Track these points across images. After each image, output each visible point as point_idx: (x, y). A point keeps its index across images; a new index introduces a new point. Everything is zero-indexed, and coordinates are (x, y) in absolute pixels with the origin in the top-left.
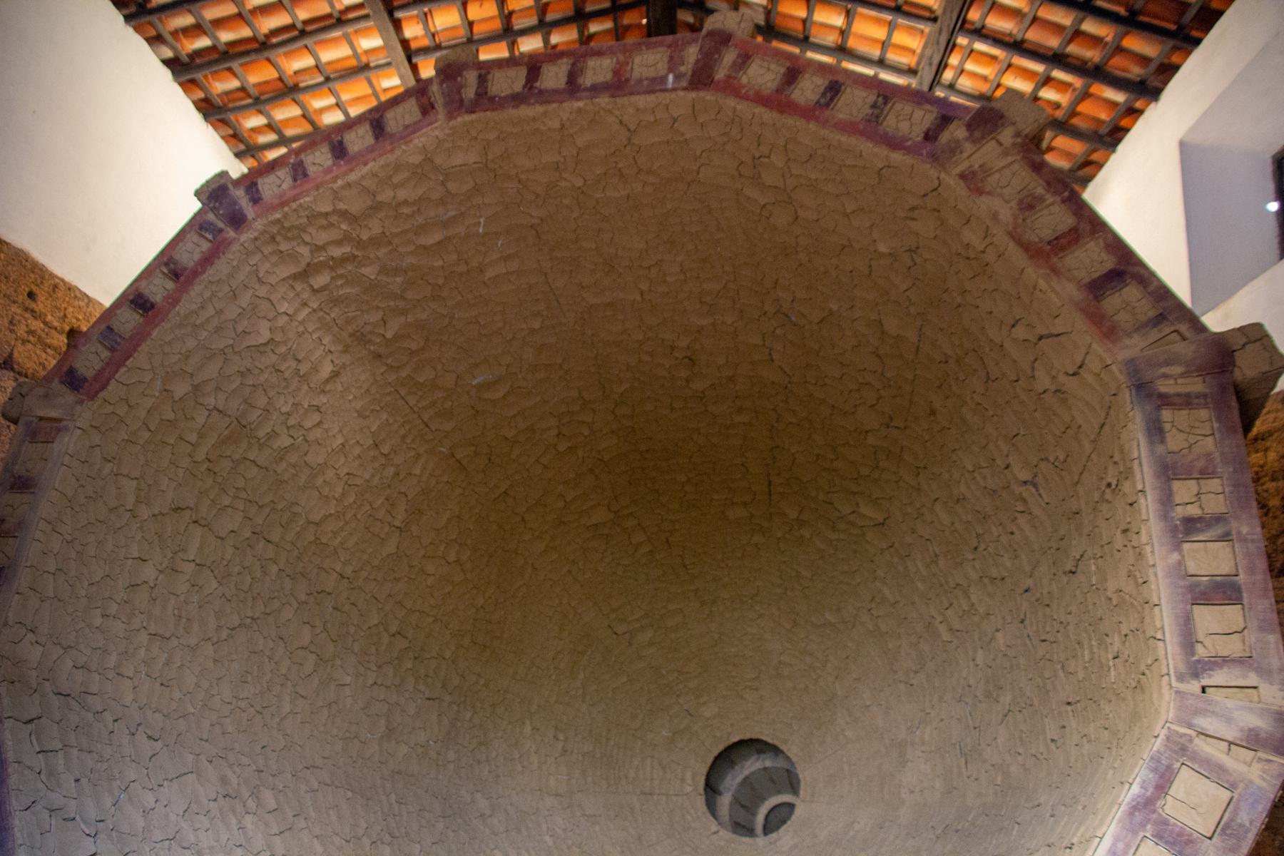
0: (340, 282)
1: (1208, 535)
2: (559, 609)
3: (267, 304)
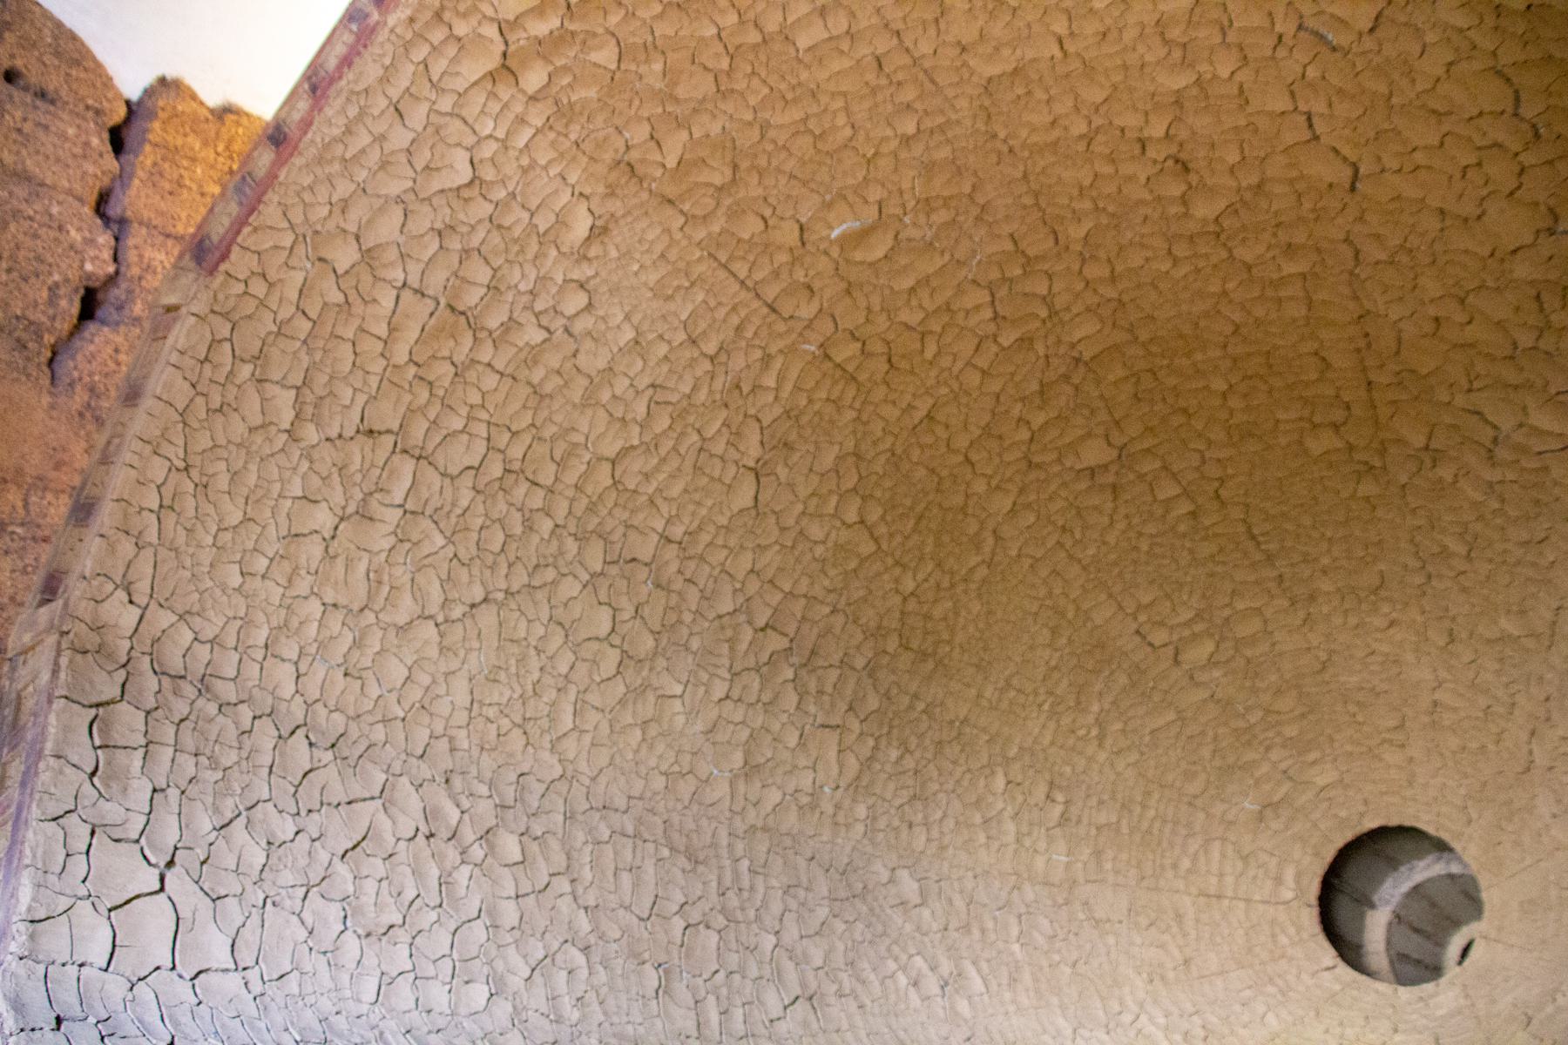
0: (566, 80)
2: (1048, 602)
3: (458, 123)
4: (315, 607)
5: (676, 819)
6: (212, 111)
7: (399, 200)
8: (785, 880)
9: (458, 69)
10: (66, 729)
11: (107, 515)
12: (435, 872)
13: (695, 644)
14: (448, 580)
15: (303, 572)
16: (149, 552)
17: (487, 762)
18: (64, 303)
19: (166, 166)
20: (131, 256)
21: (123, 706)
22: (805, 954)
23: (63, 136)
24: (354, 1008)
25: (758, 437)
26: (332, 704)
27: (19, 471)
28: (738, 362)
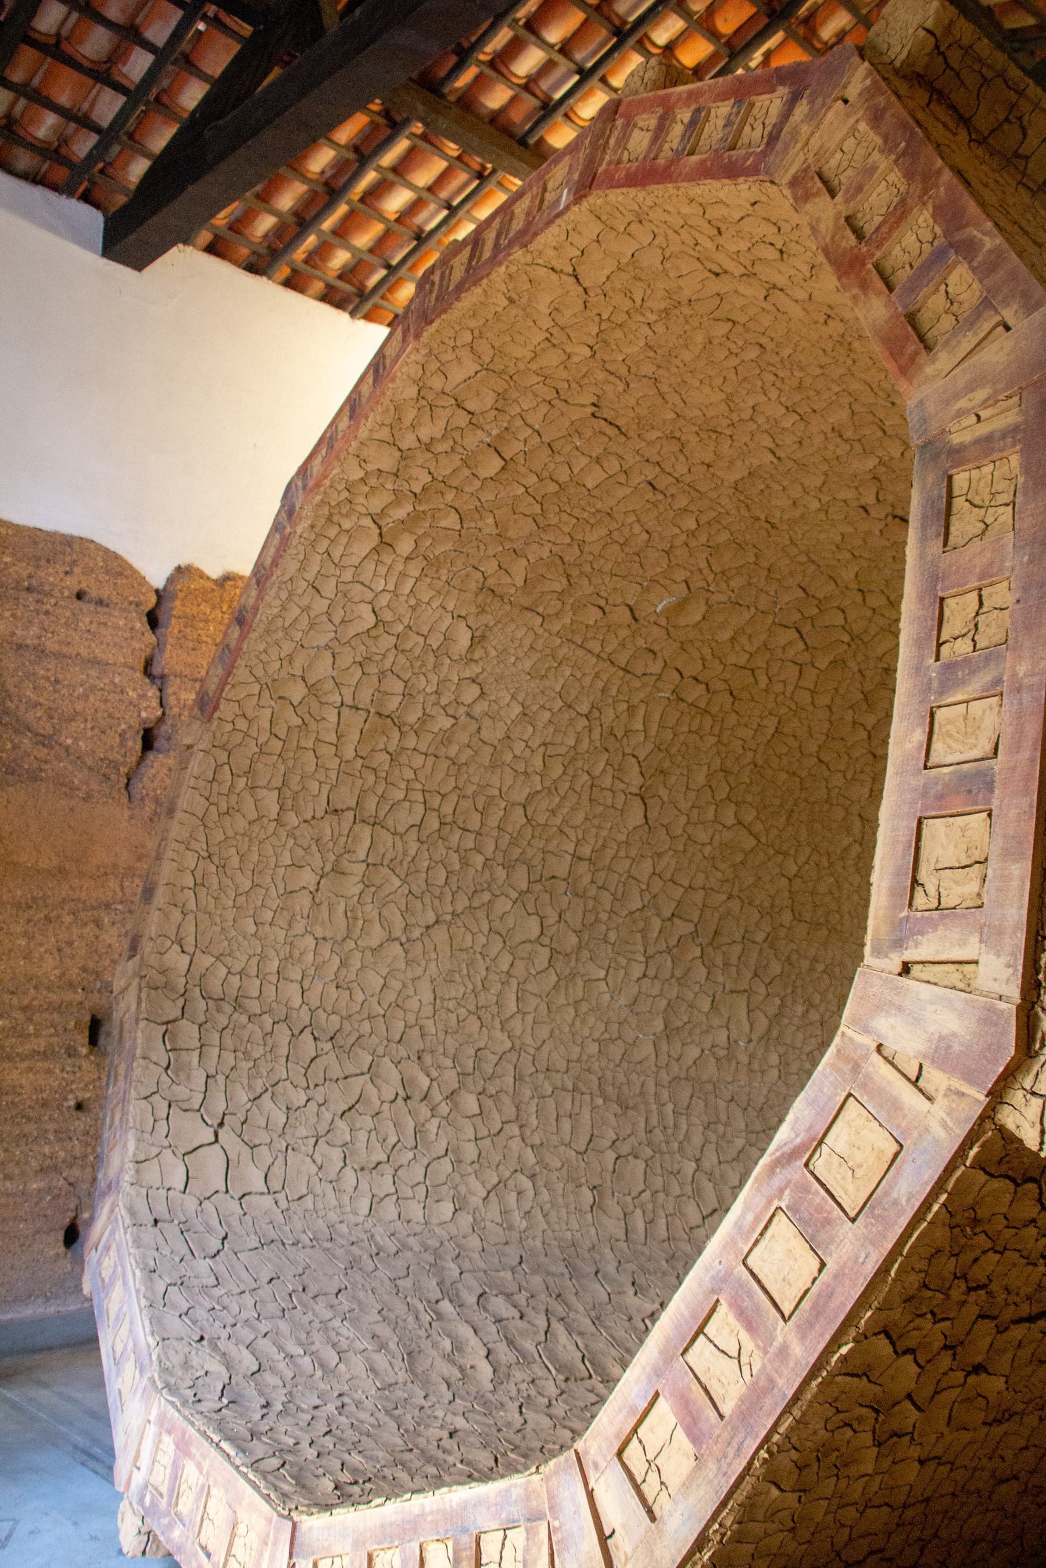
1: (970, 689)
3: (359, 586)
4: (310, 942)
5: (609, 1075)
6: (215, 581)
7: (327, 647)
8: (704, 1118)
9: (351, 550)
10: (149, 1040)
11: (161, 896)
12: (412, 1124)
13: (613, 936)
14: (407, 911)
15: (299, 918)
16: (191, 917)
17: (451, 1043)
18: (130, 743)
19: (188, 630)
20: (171, 700)
21: (184, 1022)
22: (722, 1176)
23: (117, 627)
24: (352, 1218)
25: (637, 769)
26: (329, 1009)
27: (115, 866)
28: (609, 715)
